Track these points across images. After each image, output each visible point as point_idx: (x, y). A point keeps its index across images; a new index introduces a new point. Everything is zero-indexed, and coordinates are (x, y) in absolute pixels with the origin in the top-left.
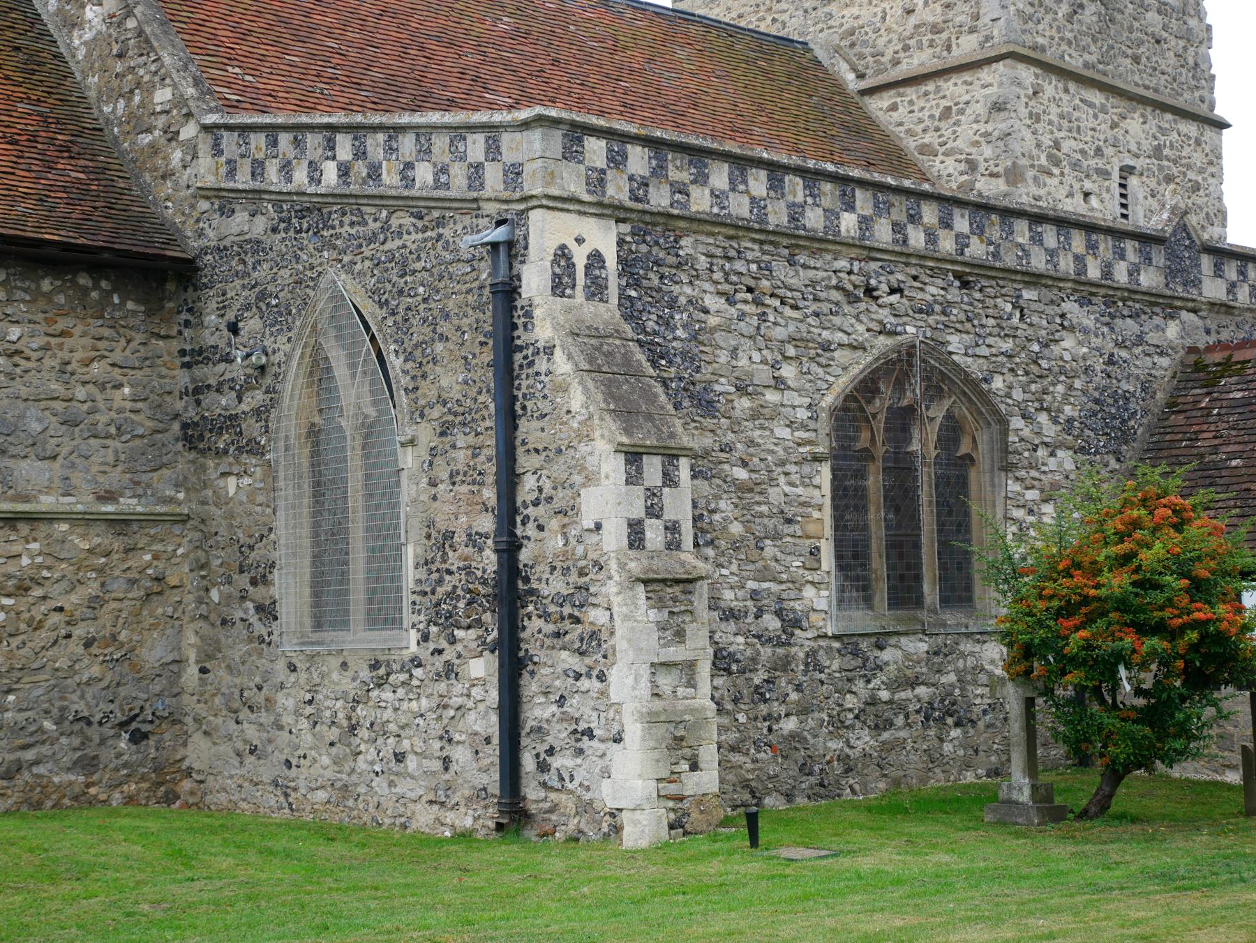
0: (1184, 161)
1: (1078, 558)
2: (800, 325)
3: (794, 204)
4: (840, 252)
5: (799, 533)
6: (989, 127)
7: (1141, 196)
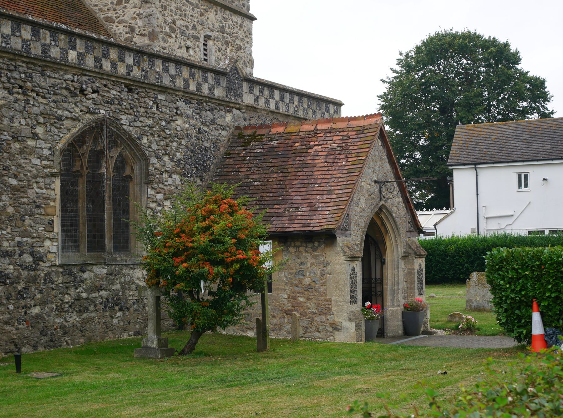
0: (234, 35)
1: (184, 228)
2: (46, 106)
3: (45, 44)
4: (68, 70)
5: (43, 213)
6: (141, 11)
7: (213, 51)
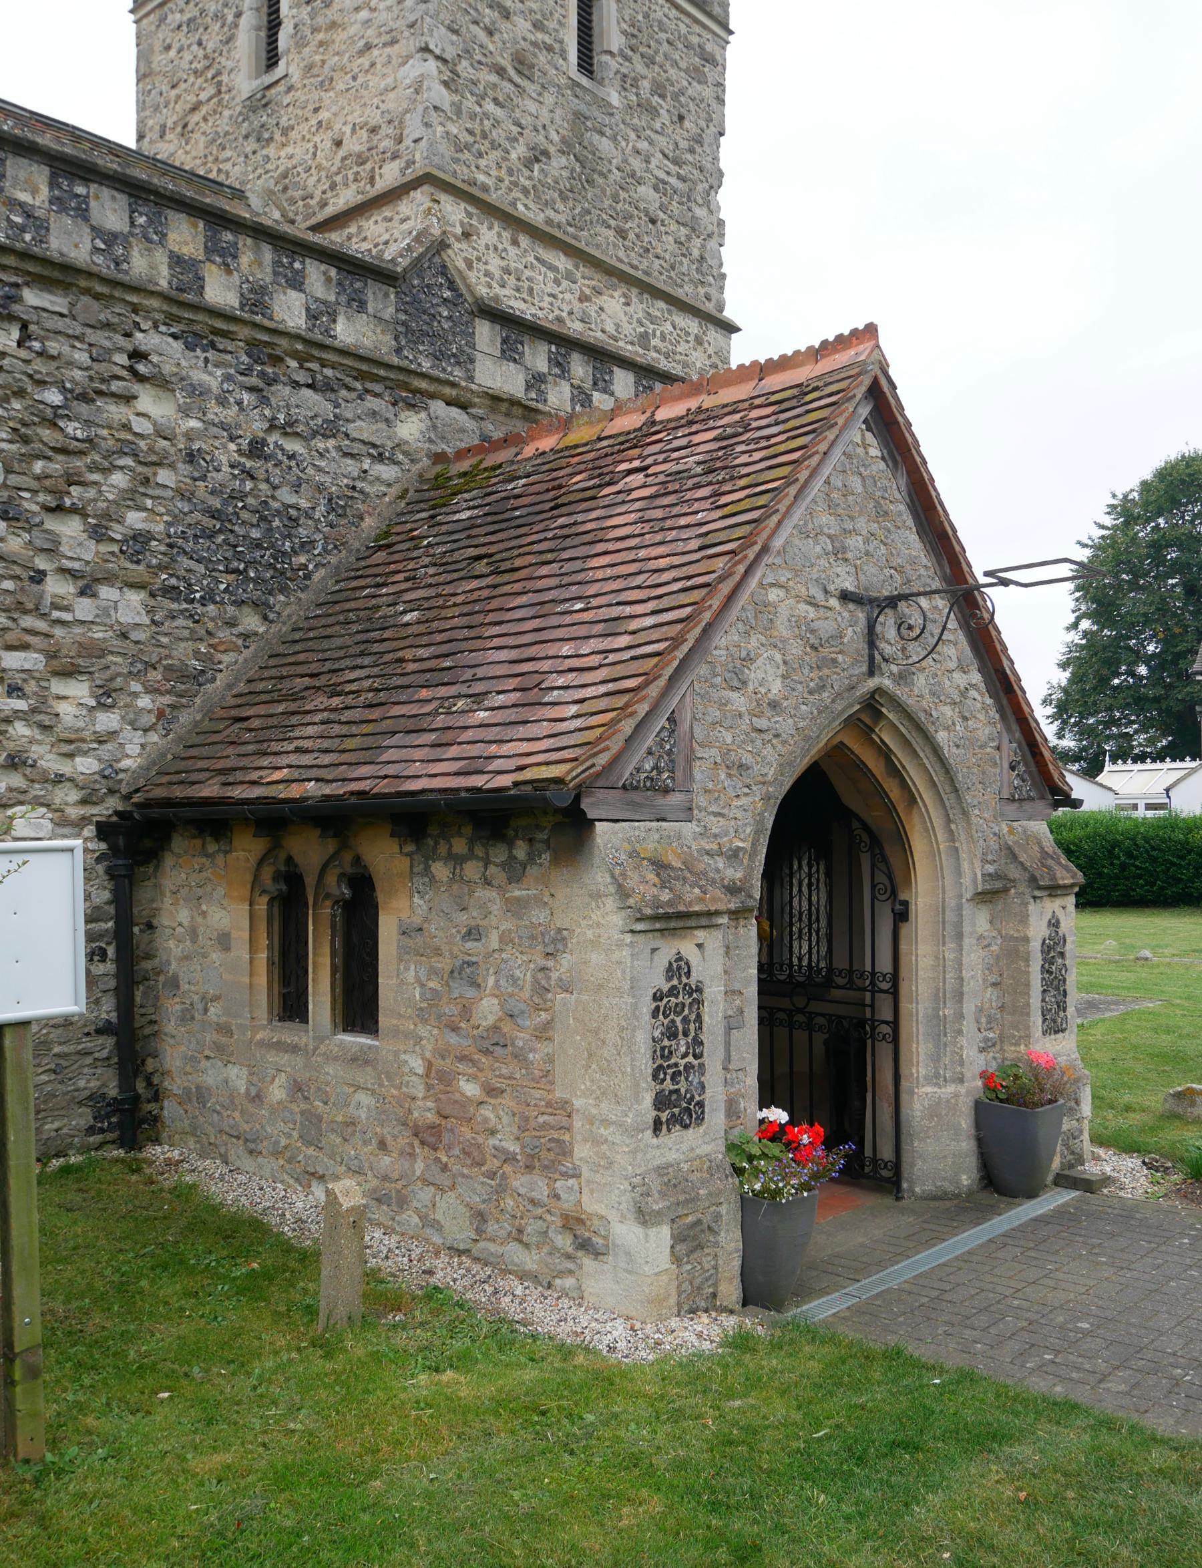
0: (678, 357)
